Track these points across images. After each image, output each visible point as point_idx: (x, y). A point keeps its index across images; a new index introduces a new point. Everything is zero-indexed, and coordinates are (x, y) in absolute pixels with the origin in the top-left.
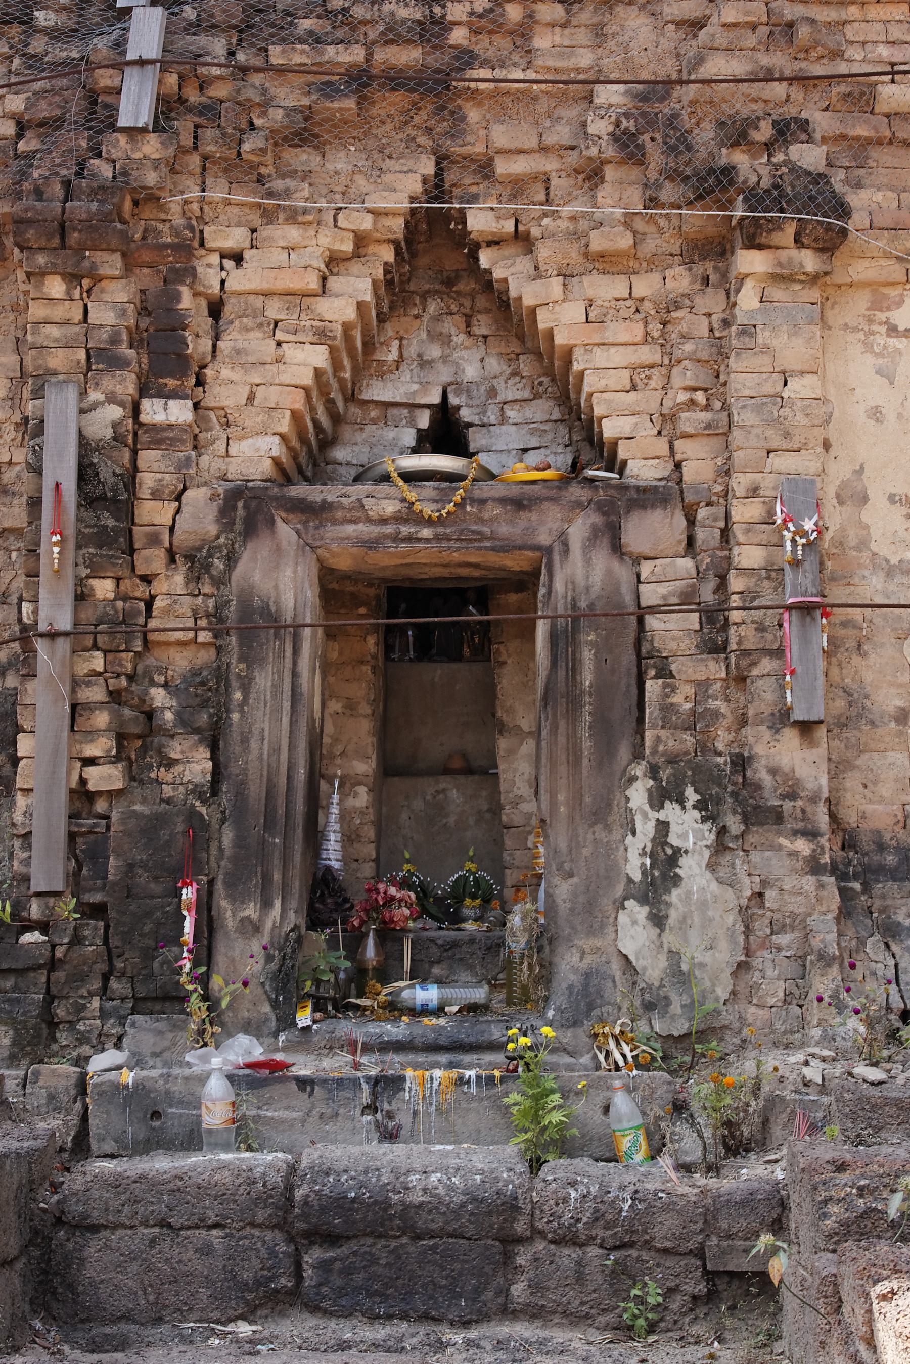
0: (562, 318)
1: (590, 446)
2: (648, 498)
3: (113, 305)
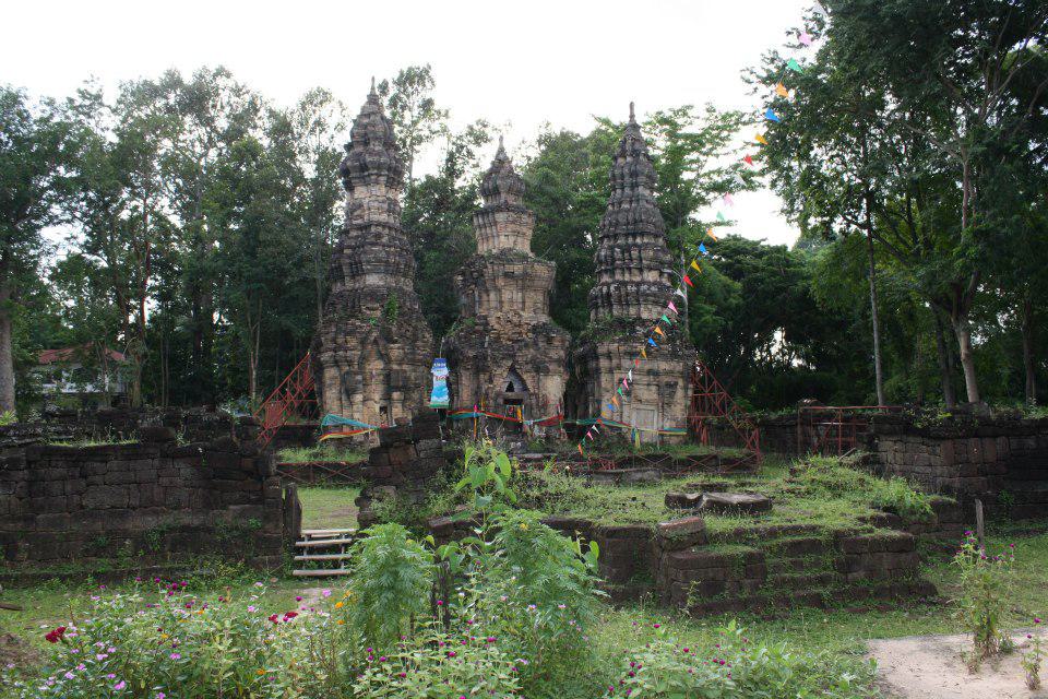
0: (525, 377)
1: (525, 388)
2: (532, 394)
3: (487, 377)
